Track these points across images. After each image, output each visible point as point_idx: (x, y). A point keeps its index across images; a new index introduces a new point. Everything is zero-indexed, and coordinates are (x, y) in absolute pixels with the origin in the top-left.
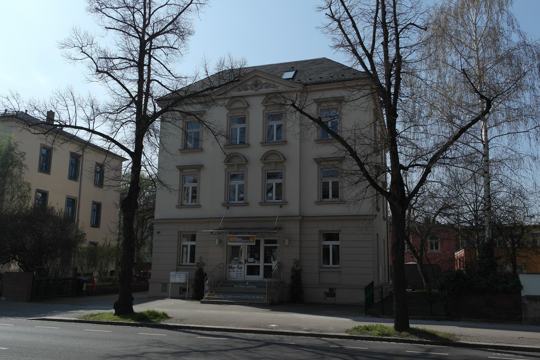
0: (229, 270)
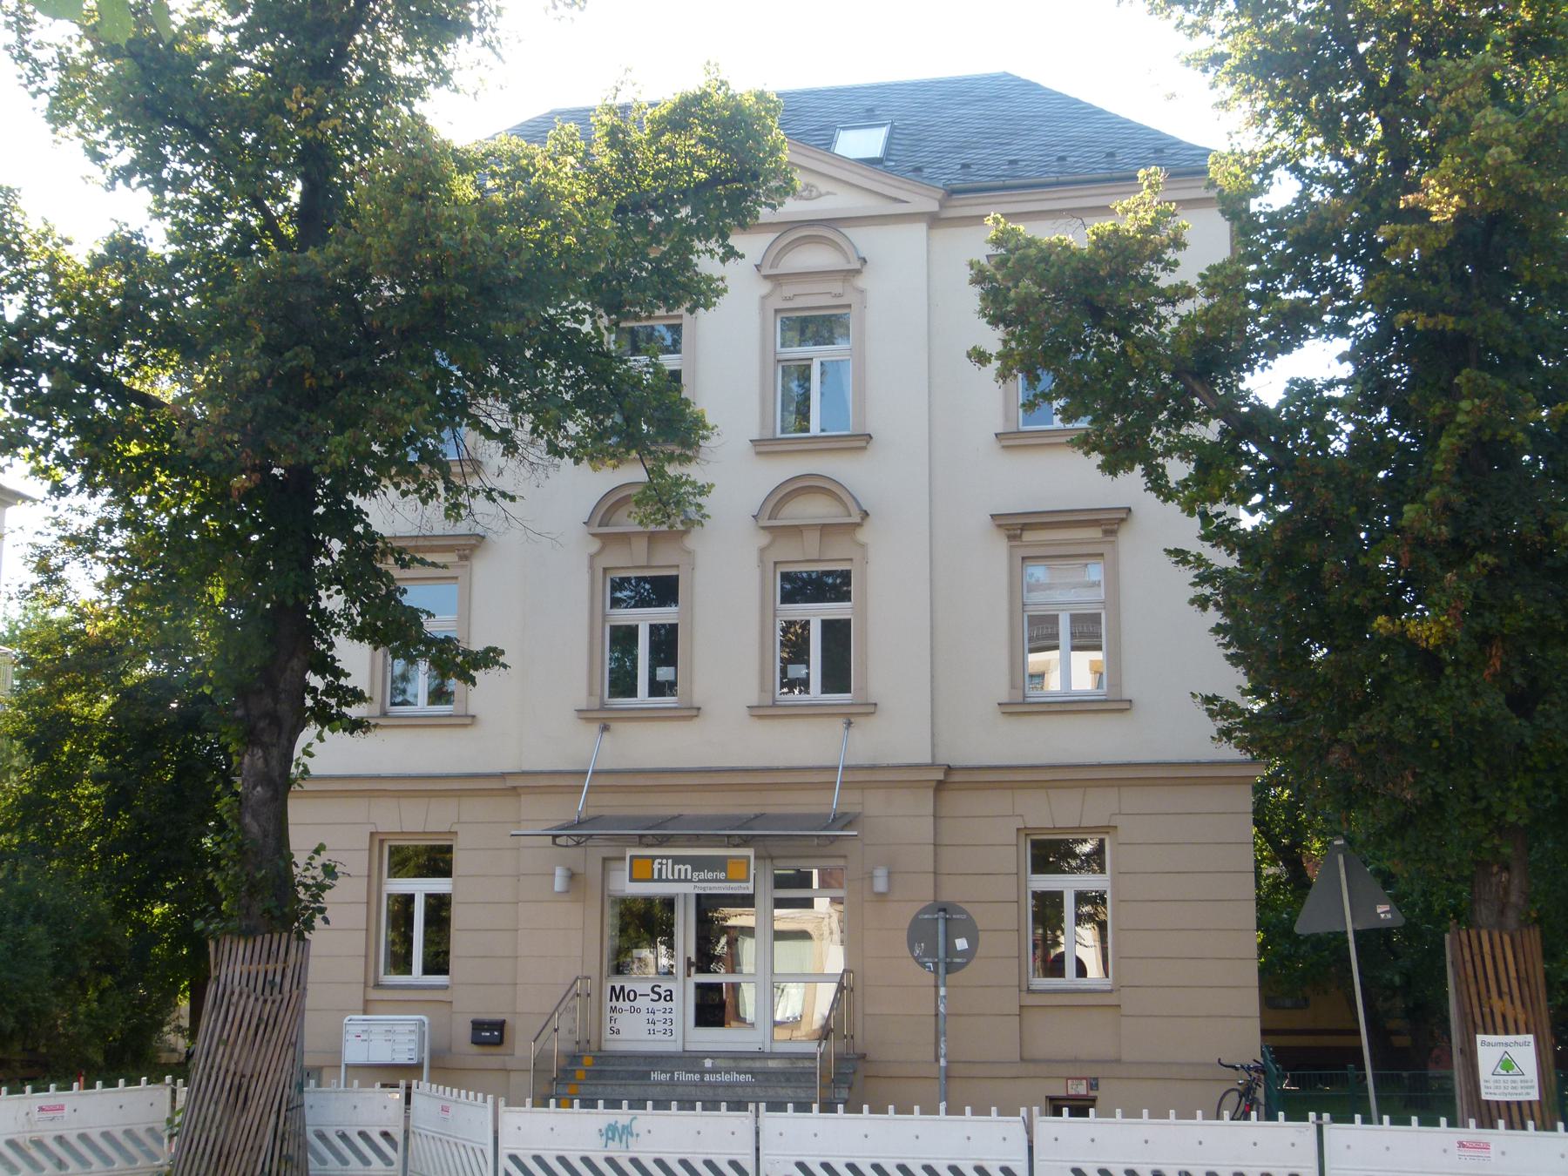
0: (614, 1003)
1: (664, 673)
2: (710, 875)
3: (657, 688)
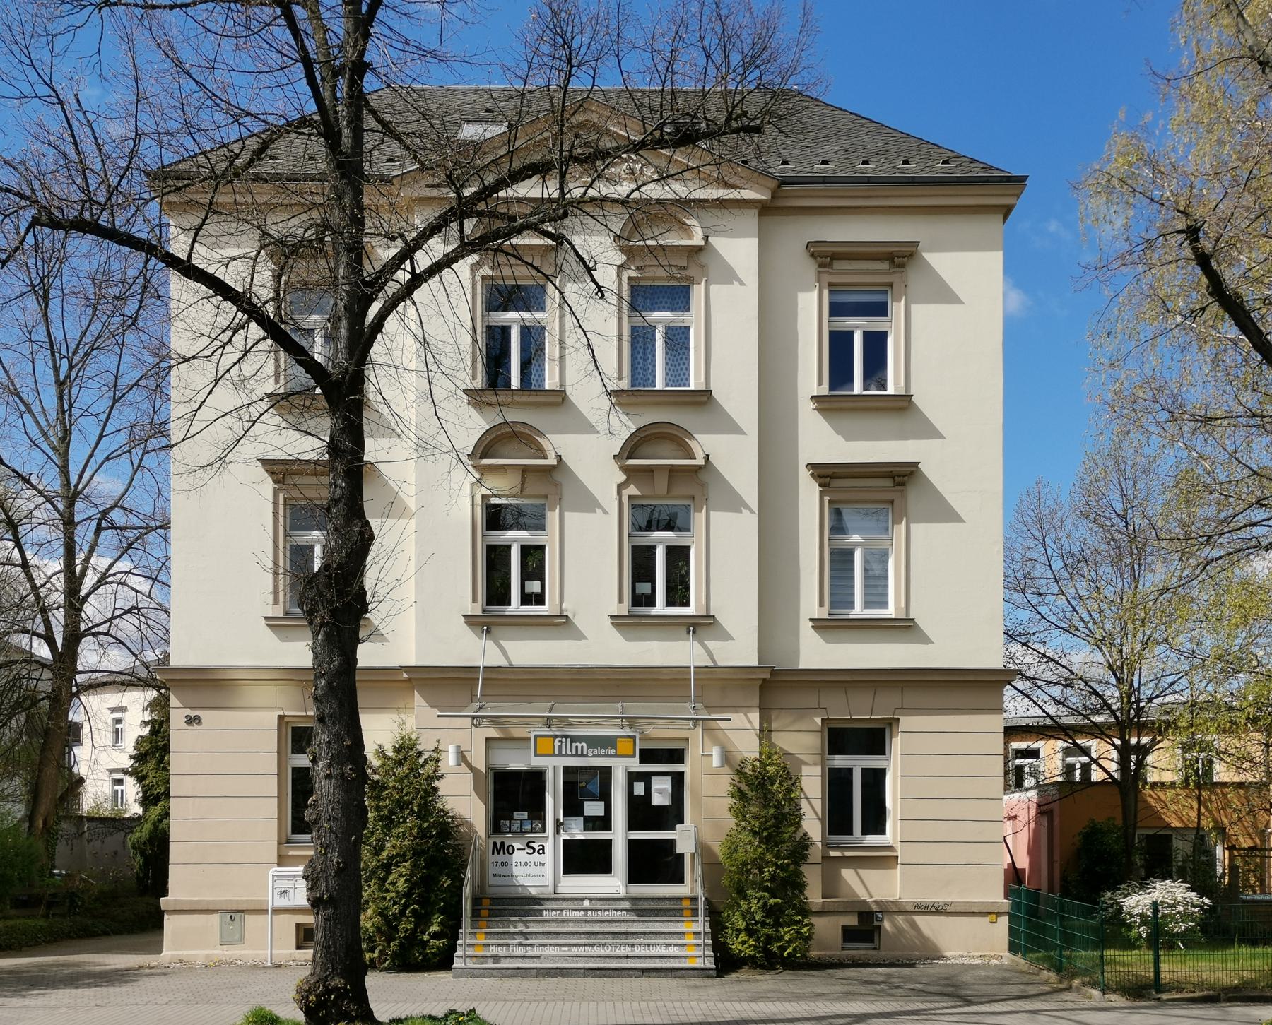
1: (534, 587)
3: (526, 599)
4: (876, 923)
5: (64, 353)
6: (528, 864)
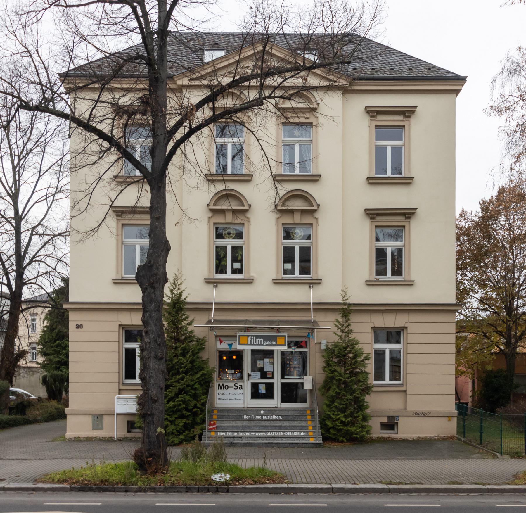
1: (237, 265)
2: (270, 343)
3: (234, 271)
4: (396, 421)
5: (16, 154)
6: (235, 394)
